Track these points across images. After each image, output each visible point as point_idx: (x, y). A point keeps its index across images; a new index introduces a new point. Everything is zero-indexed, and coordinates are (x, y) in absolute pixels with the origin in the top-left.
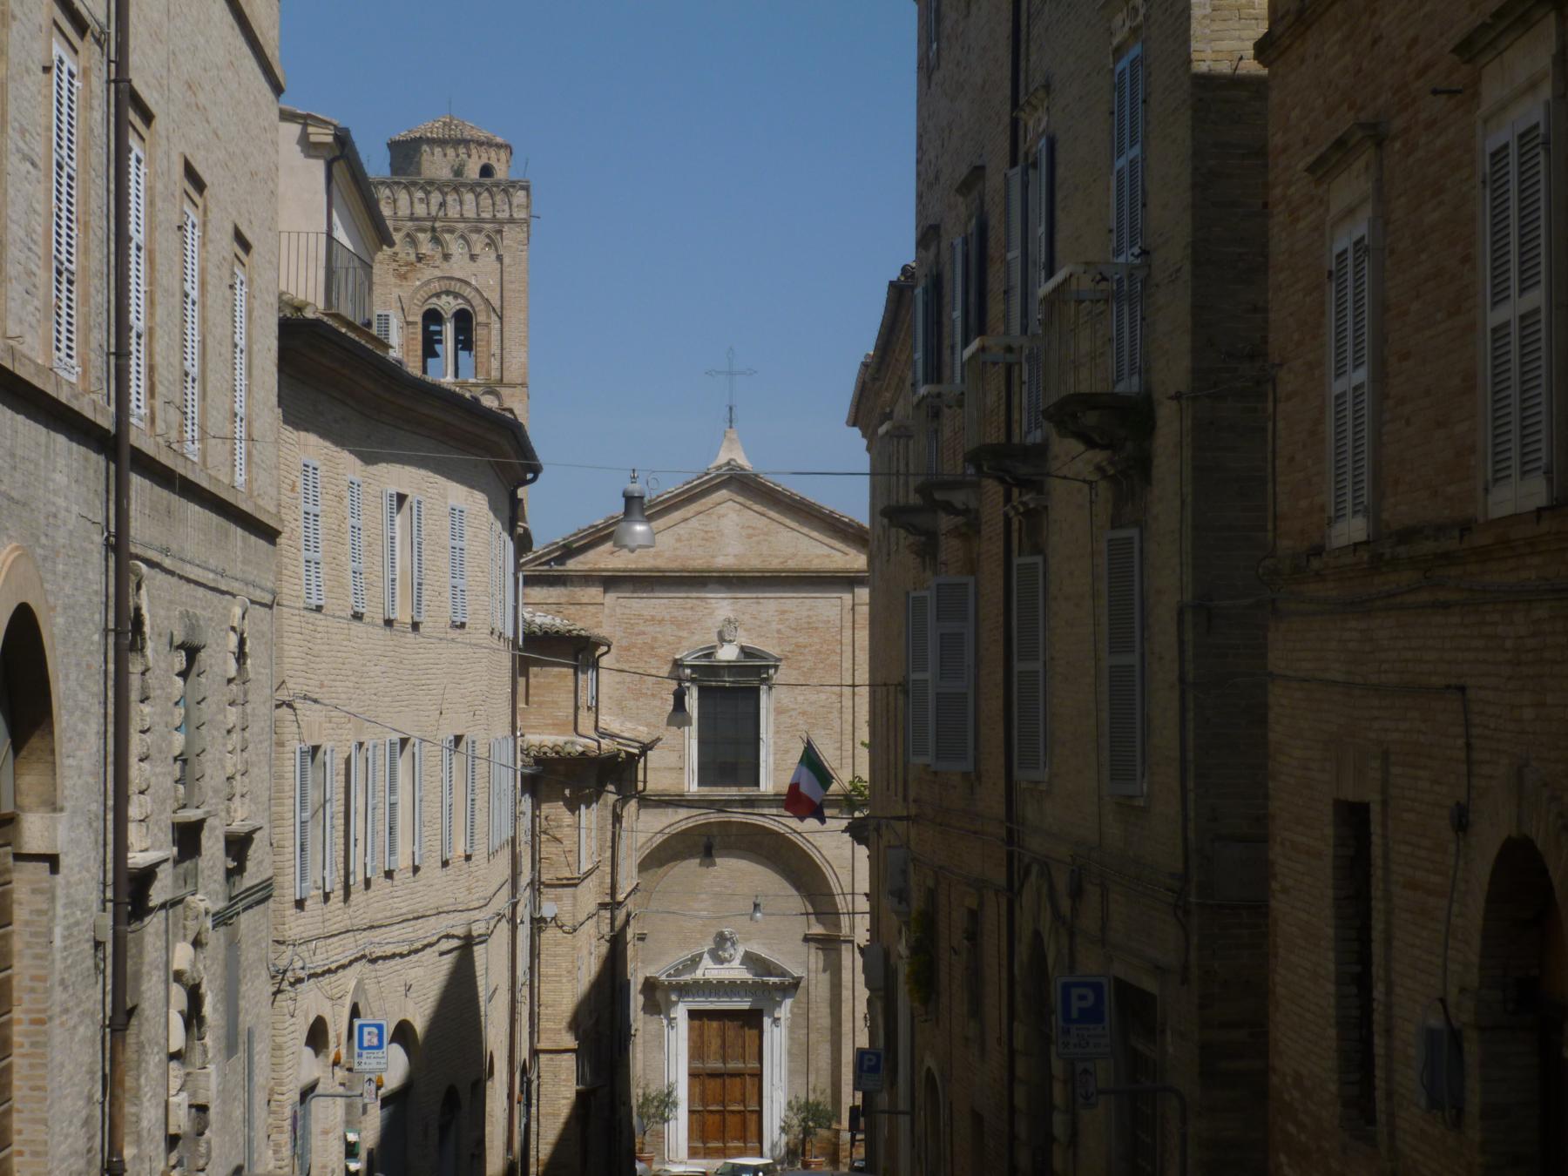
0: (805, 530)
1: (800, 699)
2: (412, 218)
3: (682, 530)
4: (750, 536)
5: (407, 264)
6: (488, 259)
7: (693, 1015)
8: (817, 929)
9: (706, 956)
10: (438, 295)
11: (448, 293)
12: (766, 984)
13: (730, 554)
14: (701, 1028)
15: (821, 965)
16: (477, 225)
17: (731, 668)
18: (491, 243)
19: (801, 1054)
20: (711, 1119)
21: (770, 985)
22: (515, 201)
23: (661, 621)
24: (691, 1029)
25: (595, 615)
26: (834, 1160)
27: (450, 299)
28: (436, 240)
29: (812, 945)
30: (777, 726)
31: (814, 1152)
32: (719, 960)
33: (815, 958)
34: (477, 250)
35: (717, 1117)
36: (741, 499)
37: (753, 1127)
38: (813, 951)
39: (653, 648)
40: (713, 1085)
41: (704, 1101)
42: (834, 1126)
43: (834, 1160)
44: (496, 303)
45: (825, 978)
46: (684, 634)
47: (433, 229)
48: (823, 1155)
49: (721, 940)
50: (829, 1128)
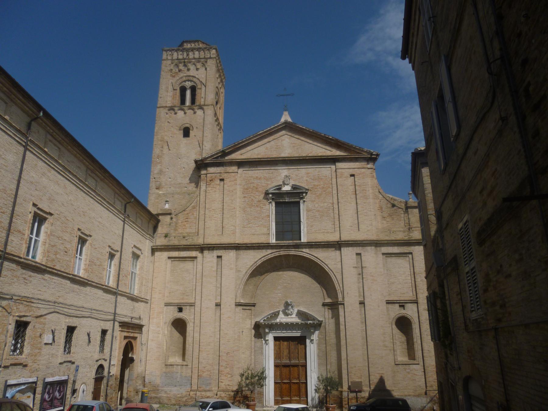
0: (315, 143)
1: (317, 205)
2: (178, 59)
3: (268, 145)
4: (294, 147)
5: (175, 73)
6: (202, 70)
7: (276, 339)
8: (328, 300)
9: (281, 313)
10: (185, 81)
11: (188, 80)
12: (306, 324)
13: (287, 152)
14: (280, 345)
15: (330, 316)
16: (199, 60)
17: (288, 193)
18: (204, 65)
19: (323, 356)
20: (284, 386)
21: (309, 325)
22: (212, 53)
23: (260, 178)
24: (275, 345)
25: (234, 176)
26: (341, 406)
27: (189, 83)
28: (185, 66)
29: (326, 307)
30: (307, 216)
31: (331, 402)
32: (286, 314)
33: (328, 313)
34: (198, 67)
35: (287, 386)
36: (290, 134)
37: (303, 390)
38: (327, 310)
39: (257, 188)
40: (285, 371)
41: (282, 379)
42: (339, 389)
43: (341, 406)
44: (204, 82)
45: (332, 321)
46: (269, 183)
47: (184, 62)
48: (335, 403)
49: (287, 305)
50: (337, 390)
